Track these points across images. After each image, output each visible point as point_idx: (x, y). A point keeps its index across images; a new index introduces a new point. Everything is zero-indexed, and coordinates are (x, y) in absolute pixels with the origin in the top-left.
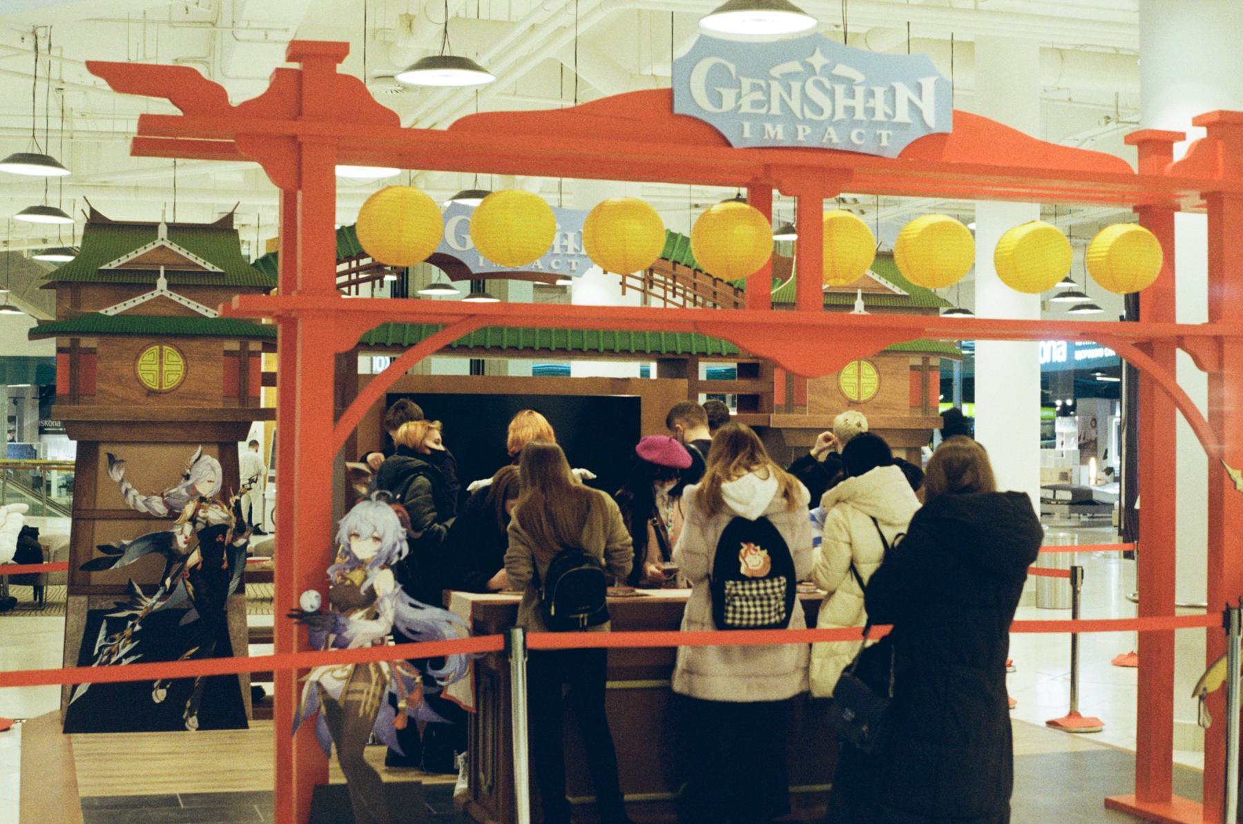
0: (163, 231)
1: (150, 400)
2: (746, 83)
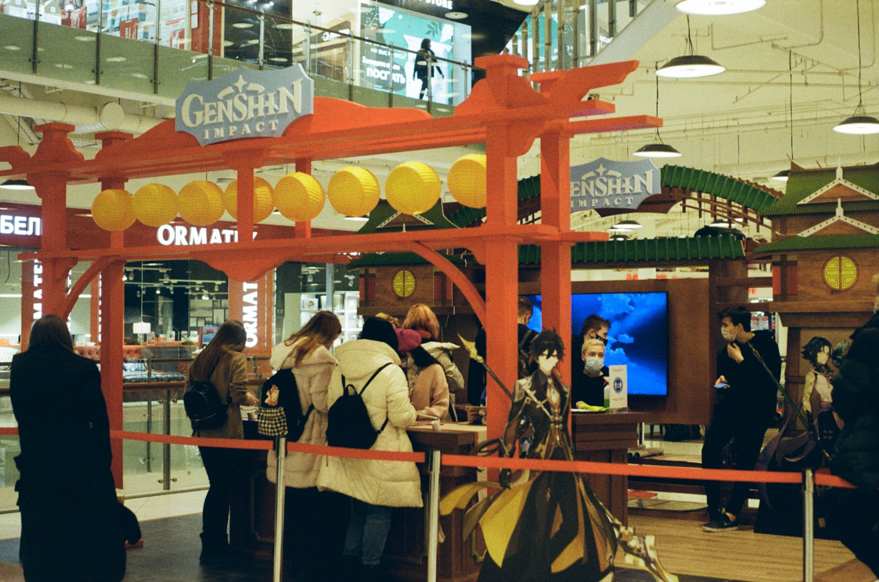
0: (839, 173)
1: (833, 297)
2: (207, 105)
